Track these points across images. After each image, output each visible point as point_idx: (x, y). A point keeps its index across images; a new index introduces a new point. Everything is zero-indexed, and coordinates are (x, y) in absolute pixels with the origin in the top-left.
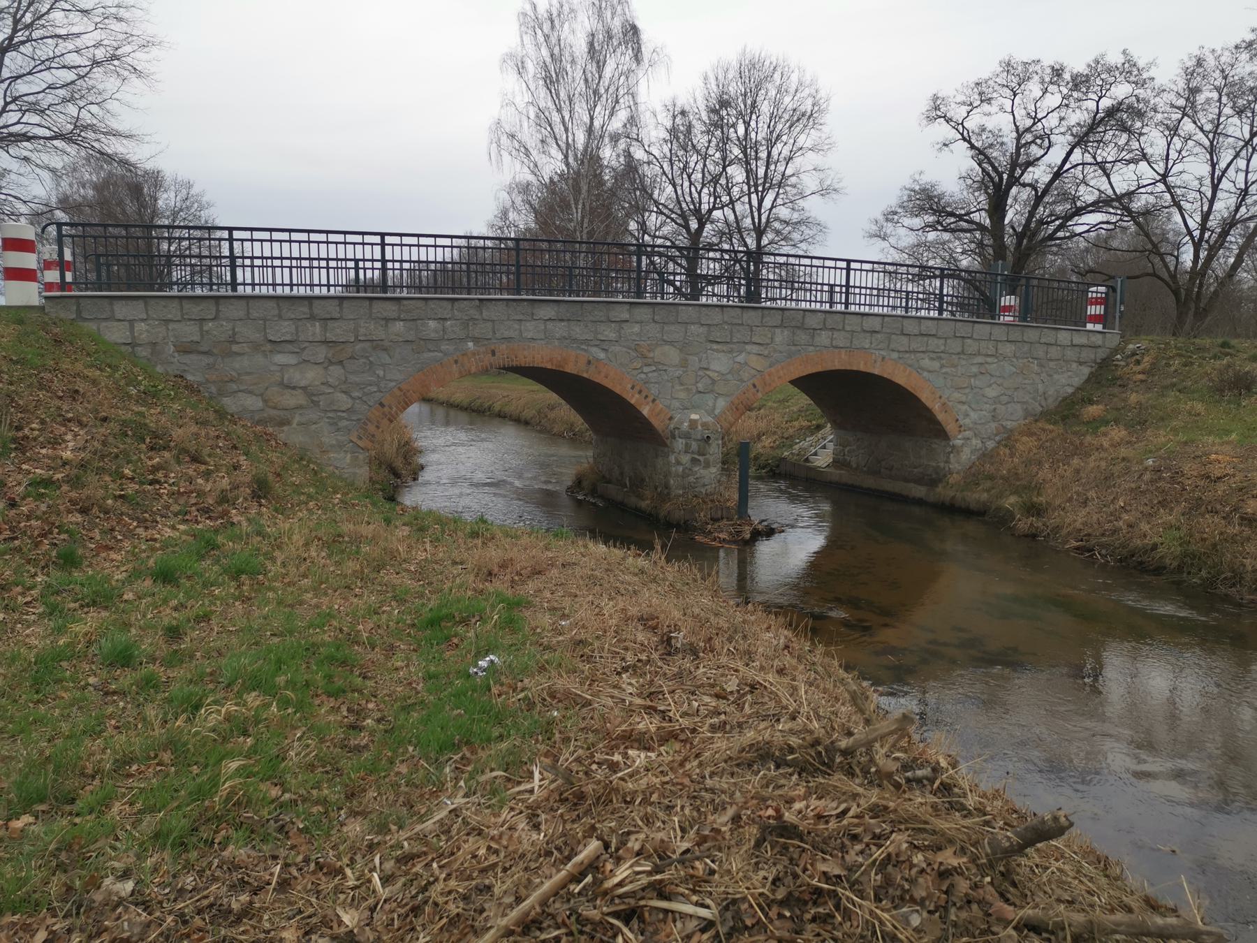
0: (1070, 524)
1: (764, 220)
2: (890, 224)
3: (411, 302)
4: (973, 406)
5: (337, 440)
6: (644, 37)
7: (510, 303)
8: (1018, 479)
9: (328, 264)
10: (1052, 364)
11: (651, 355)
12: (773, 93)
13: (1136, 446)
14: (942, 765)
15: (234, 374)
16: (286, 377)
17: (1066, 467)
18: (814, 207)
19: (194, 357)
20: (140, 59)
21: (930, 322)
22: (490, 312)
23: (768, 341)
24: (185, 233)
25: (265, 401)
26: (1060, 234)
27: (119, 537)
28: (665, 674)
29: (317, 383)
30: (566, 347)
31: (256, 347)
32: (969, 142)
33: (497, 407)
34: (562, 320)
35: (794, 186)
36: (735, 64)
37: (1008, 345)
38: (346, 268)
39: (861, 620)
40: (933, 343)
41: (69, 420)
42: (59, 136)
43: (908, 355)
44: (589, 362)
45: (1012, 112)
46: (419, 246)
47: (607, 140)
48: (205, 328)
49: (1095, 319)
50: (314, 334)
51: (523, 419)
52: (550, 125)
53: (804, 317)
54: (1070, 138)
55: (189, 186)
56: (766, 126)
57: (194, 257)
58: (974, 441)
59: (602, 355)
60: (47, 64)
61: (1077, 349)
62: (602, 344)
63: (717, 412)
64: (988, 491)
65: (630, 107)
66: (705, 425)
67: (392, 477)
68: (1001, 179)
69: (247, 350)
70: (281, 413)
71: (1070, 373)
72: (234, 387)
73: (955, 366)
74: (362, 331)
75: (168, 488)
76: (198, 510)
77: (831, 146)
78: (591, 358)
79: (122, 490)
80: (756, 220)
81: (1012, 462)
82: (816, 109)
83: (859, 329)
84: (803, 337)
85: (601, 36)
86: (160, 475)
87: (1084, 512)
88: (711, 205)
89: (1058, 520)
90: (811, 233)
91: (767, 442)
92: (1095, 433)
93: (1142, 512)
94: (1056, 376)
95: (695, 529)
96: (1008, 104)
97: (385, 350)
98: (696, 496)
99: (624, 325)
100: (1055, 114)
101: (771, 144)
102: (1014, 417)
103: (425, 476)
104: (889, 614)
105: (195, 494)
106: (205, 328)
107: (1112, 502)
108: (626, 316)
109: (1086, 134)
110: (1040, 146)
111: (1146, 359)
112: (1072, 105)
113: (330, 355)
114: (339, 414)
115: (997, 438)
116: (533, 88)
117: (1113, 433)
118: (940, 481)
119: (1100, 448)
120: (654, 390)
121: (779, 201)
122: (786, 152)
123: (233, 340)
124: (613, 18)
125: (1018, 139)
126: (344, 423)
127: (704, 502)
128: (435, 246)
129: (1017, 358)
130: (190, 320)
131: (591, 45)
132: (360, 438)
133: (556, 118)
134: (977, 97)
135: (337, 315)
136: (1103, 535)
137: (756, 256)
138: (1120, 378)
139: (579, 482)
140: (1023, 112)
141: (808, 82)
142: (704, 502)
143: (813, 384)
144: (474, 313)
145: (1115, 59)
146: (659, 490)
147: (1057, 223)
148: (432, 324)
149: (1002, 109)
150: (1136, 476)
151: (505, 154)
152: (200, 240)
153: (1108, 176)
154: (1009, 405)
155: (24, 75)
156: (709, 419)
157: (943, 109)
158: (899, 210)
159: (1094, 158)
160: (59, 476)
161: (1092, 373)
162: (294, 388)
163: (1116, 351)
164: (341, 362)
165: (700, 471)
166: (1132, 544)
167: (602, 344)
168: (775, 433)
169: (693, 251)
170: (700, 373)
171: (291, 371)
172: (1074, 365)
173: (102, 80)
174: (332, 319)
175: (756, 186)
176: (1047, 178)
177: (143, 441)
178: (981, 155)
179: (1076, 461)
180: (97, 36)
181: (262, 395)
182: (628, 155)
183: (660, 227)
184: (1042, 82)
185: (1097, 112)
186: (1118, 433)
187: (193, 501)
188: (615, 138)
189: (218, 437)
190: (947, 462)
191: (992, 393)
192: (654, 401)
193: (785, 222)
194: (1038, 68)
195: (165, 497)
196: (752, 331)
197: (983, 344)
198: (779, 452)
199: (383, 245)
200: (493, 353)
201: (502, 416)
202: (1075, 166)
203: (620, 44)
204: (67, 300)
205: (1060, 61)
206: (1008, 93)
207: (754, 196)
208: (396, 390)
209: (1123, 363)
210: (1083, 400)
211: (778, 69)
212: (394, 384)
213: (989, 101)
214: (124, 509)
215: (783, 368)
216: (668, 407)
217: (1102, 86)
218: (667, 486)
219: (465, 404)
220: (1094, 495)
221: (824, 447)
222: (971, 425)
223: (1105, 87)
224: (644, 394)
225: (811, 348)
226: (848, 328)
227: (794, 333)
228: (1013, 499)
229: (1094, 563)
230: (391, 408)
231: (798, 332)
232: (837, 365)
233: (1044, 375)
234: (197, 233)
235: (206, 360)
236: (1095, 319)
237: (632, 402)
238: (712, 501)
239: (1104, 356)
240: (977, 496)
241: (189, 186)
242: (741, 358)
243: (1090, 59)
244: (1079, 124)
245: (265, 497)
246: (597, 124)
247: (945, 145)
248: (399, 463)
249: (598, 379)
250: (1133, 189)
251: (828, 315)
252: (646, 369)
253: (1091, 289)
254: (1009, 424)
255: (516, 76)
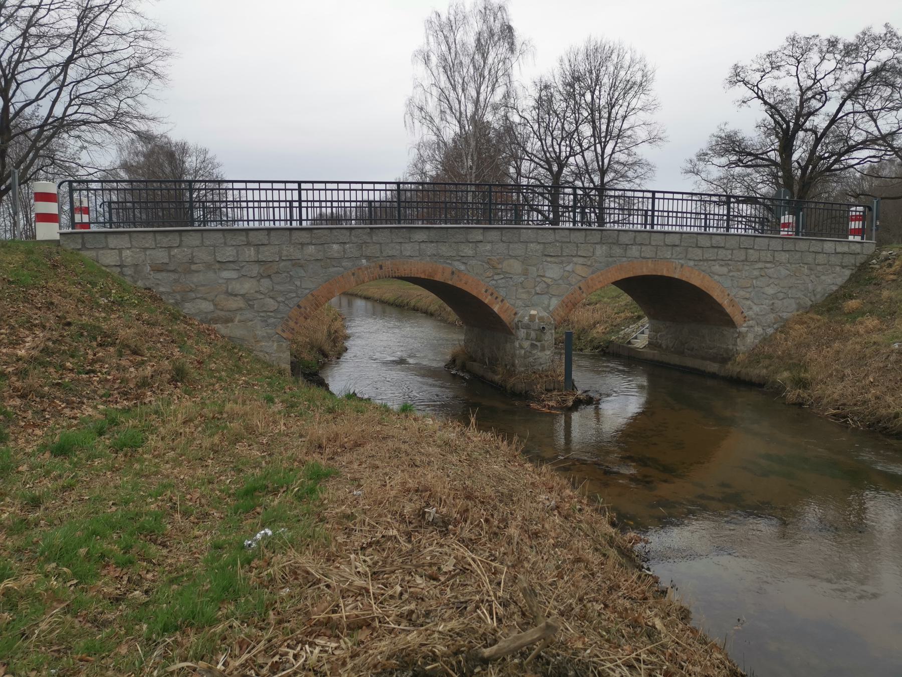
0: (829, 396)
1: (606, 161)
2: (701, 163)
3: (320, 231)
4: (755, 301)
5: (267, 333)
6: (516, 34)
7: (393, 230)
8: (791, 359)
9: (332, 204)
10: (819, 268)
11: (500, 266)
12: (611, 69)
13: (886, 332)
14: (657, 627)
15: (193, 286)
16: (230, 287)
17: (829, 349)
18: (643, 152)
19: (164, 274)
20: (159, 65)
21: (719, 237)
22: (377, 237)
23: (590, 254)
24: (203, 185)
25: (215, 305)
26: (836, 166)
27: (47, 416)
28: (401, 550)
29: (252, 291)
30: (436, 262)
31: (209, 266)
32: (763, 99)
33: (413, 303)
34: (432, 242)
35: (629, 137)
36: (583, 49)
37: (783, 253)
38: (240, 207)
39: (645, 476)
40: (722, 253)
41: (36, 326)
42: (104, 121)
43: (702, 263)
44: (453, 273)
45: (797, 75)
46: (374, 190)
47: (489, 109)
48: (172, 253)
49: (855, 232)
50: (250, 256)
51: (429, 311)
52: (448, 100)
53: (618, 236)
54: (842, 93)
55: (206, 152)
56: (606, 94)
57: (209, 202)
58: (756, 329)
59: (462, 267)
60: (99, 71)
61: (840, 256)
62: (463, 259)
63: (551, 308)
64: (767, 368)
65: (506, 84)
66: (541, 319)
67: (321, 357)
68: (788, 126)
69: (202, 268)
70: (227, 313)
71: (834, 275)
72: (193, 295)
73: (739, 270)
74: (285, 253)
75: (101, 376)
76: (119, 393)
77: (656, 106)
78: (454, 269)
79: (61, 379)
80: (600, 163)
81: (786, 344)
82: (645, 79)
83: (662, 244)
84: (617, 251)
85: (485, 35)
86: (97, 366)
87: (840, 386)
88: (568, 153)
89: (820, 392)
90: (643, 171)
91: (600, 329)
92: (853, 322)
93: (887, 387)
94: (823, 277)
95: (532, 399)
96: (793, 70)
97: (301, 266)
98: (534, 373)
99: (479, 245)
100: (831, 76)
101: (611, 105)
102: (788, 309)
103: (347, 356)
104: (669, 471)
105: (119, 381)
106: (172, 253)
107: (864, 378)
108: (480, 238)
109: (856, 89)
110: (819, 101)
111: (897, 263)
112: (845, 68)
113: (261, 271)
114: (268, 314)
115: (775, 326)
116: (436, 74)
117: (867, 322)
118: (730, 359)
119: (857, 334)
120: (502, 293)
121: (617, 149)
122: (622, 112)
123: (192, 262)
124: (494, 21)
125: (802, 96)
126: (272, 320)
127: (540, 377)
128: (362, 190)
129: (791, 264)
130: (161, 247)
131: (479, 40)
132: (284, 331)
133: (452, 95)
134: (769, 65)
135: (266, 242)
136: (855, 405)
137: (602, 189)
138: (875, 278)
139: (453, 361)
140: (805, 75)
141: (638, 60)
142: (540, 377)
143: (630, 285)
144: (366, 238)
145: (879, 30)
146: (508, 367)
147: (833, 158)
148: (335, 247)
149: (789, 74)
150: (884, 356)
151: (416, 122)
152: (212, 190)
153: (875, 121)
154: (785, 301)
155: (83, 80)
156: (545, 314)
157: (742, 75)
158: (710, 152)
159: (864, 107)
160: (10, 369)
161: (852, 275)
162: (236, 295)
163: (871, 257)
164: (269, 276)
165: (537, 353)
166: (878, 413)
167: (463, 259)
168: (606, 322)
169: (556, 188)
170: (538, 279)
171: (234, 283)
172: (838, 269)
173: (136, 82)
174: (262, 245)
175: (600, 137)
176: (824, 125)
177: (96, 340)
178: (773, 109)
179: (837, 345)
180: (131, 51)
181: (213, 301)
182: (506, 118)
183: (533, 170)
184: (821, 51)
185: (865, 72)
186: (871, 322)
187: (116, 386)
188: (495, 108)
189: (162, 334)
190: (735, 344)
191: (770, 291)
192: (502, 301)
193: (623, 163)
194: (817, 41)
195: (96, 383)
196: (577, 247)
197: (763, 254)
198: (608, 336)
199: (300, 190)
200: (381, 267)
201: (415, 309)
202: (847, 115)
203: (499, 39)
204: (76, 235)
205: (835, 35)
206: (793, 61)
207: (598, 146)
208: (309, 296)
209: (877, 266)
210: (844, 295)
211: (615, 51)
212: (307, 291)
213: (778, 68)
214: (58, 394)
215: (602, 275)
216: (513, 305)
217: (868, 52)
218: (513, 365)
219: (392, 300)
220: (849, 372)
221: (643, 333)
222: (754, 316)
223: (871, 52)
224: (495, 296)
225: (624, 259)
226: (653, 243)
227: (611, 248)
228: (786, 374)
229: (847, 428)
230: (306, 309)
231: (614, 247)
232: (645, 272)
233: (813, 276)
234: (211, 185)
235: (173, 276)
236: (855, 232)
237: (486, 302)
238: (547, 376)
239: (863, 261)
240: (758, 372)
241: (206, 152)
242: (569, 268)
243: (858, 31)
244: (850, 82)
245: (182, 381)
246: (482, 98)
247: (744, 102)
248: (327, 347)
249: (460, 285)
250: (894, 130)
251: (637, 234)
252: (496, 277)
253: (852, 209)
254: (785, 315)
255: (424, 66)
